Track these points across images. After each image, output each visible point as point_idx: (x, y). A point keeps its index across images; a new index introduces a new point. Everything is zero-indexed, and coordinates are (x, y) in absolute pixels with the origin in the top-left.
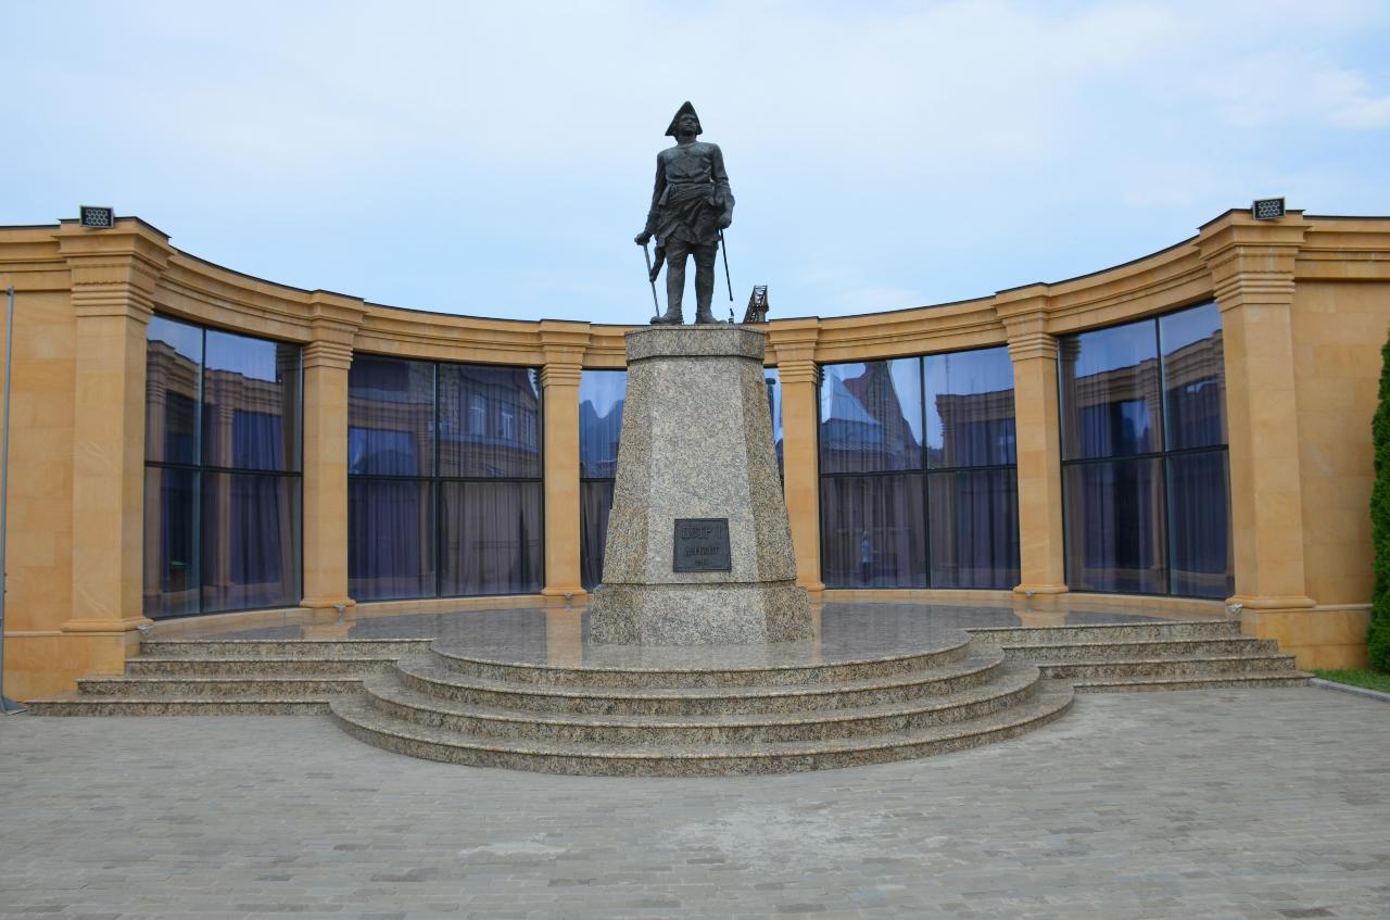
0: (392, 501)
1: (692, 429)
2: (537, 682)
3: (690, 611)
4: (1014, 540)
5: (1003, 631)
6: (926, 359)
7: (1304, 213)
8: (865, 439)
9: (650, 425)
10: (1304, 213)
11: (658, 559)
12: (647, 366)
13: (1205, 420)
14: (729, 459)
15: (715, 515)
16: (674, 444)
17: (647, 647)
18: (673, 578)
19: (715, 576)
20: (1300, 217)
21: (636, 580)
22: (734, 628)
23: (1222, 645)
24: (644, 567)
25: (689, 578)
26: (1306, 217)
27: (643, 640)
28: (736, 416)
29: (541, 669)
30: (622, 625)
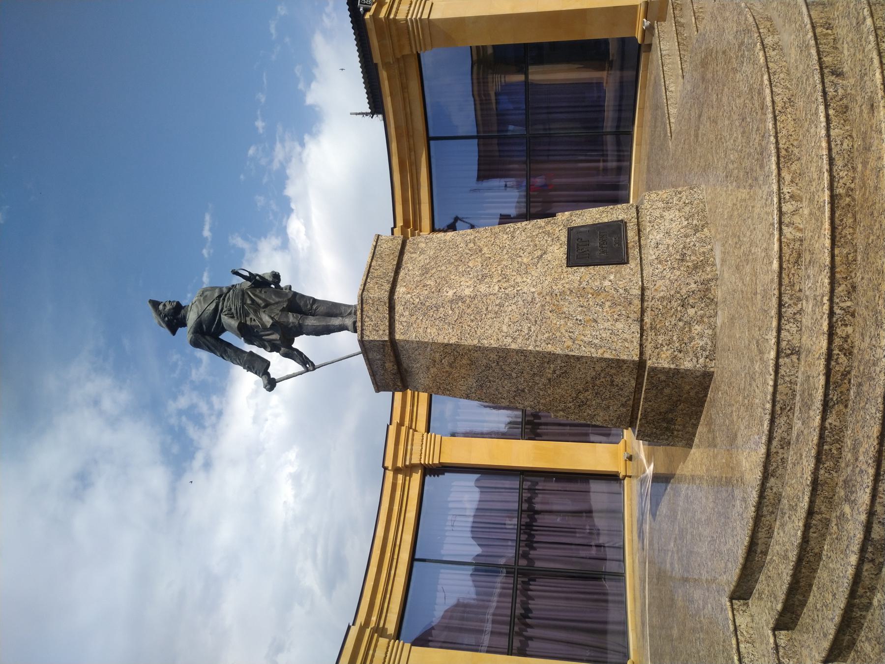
0: (549, 150)
1: (471, 264)
2: (800, 230)
3: (671, 242)
4: (567, 438)
5: (670, 128)
6: (431, 134)
7: (351, 624)
8: (497, 154)
9: (461, 298)
10: (351, 624)
11: (612, 277)
12: (399, 308)
13: (499, 151)
14: (505, 237)
15: (564, 239)
16: (484, 276)
17: (718, 272)
18: (633, 264)
19: (631, 234)
20: (352, 627)
21: (637, 302)
22: (687, 209)
23: (677, 12)
24: (621, 291)
25: (634, 252)
26: (354, 624)
27: (709, 276)
28: (463, 235)
29: (780, 223)
30: (691, 311)
